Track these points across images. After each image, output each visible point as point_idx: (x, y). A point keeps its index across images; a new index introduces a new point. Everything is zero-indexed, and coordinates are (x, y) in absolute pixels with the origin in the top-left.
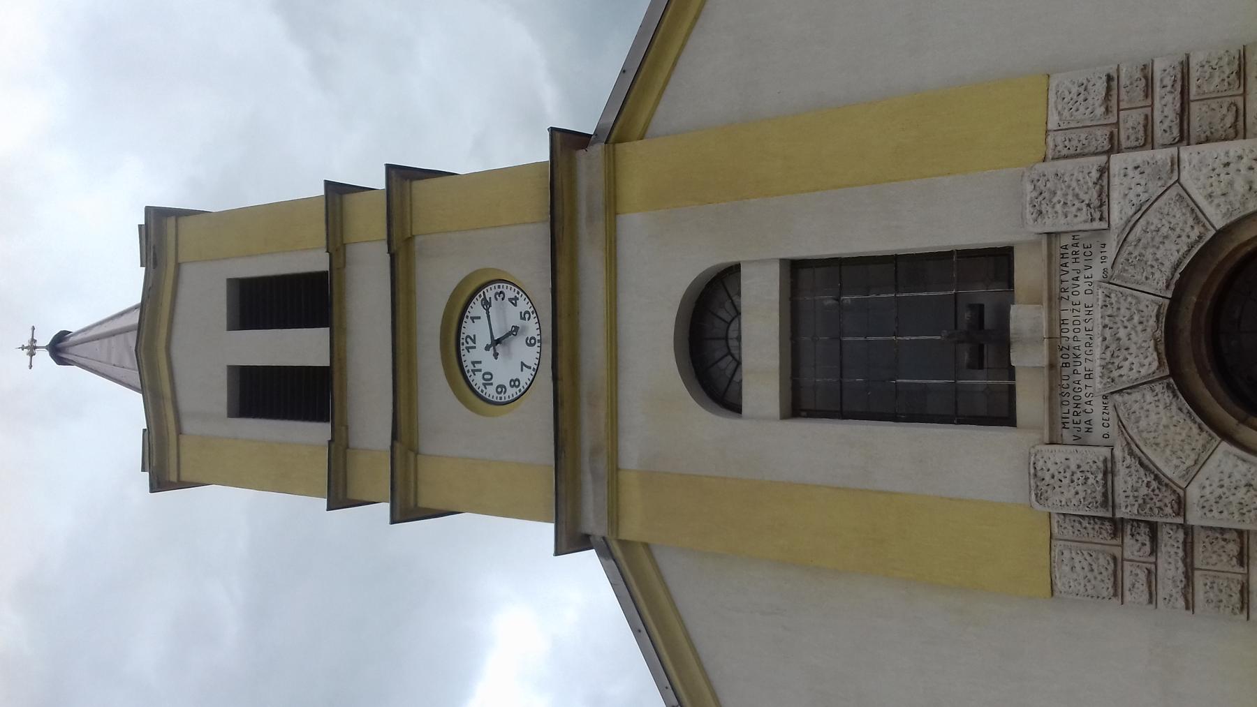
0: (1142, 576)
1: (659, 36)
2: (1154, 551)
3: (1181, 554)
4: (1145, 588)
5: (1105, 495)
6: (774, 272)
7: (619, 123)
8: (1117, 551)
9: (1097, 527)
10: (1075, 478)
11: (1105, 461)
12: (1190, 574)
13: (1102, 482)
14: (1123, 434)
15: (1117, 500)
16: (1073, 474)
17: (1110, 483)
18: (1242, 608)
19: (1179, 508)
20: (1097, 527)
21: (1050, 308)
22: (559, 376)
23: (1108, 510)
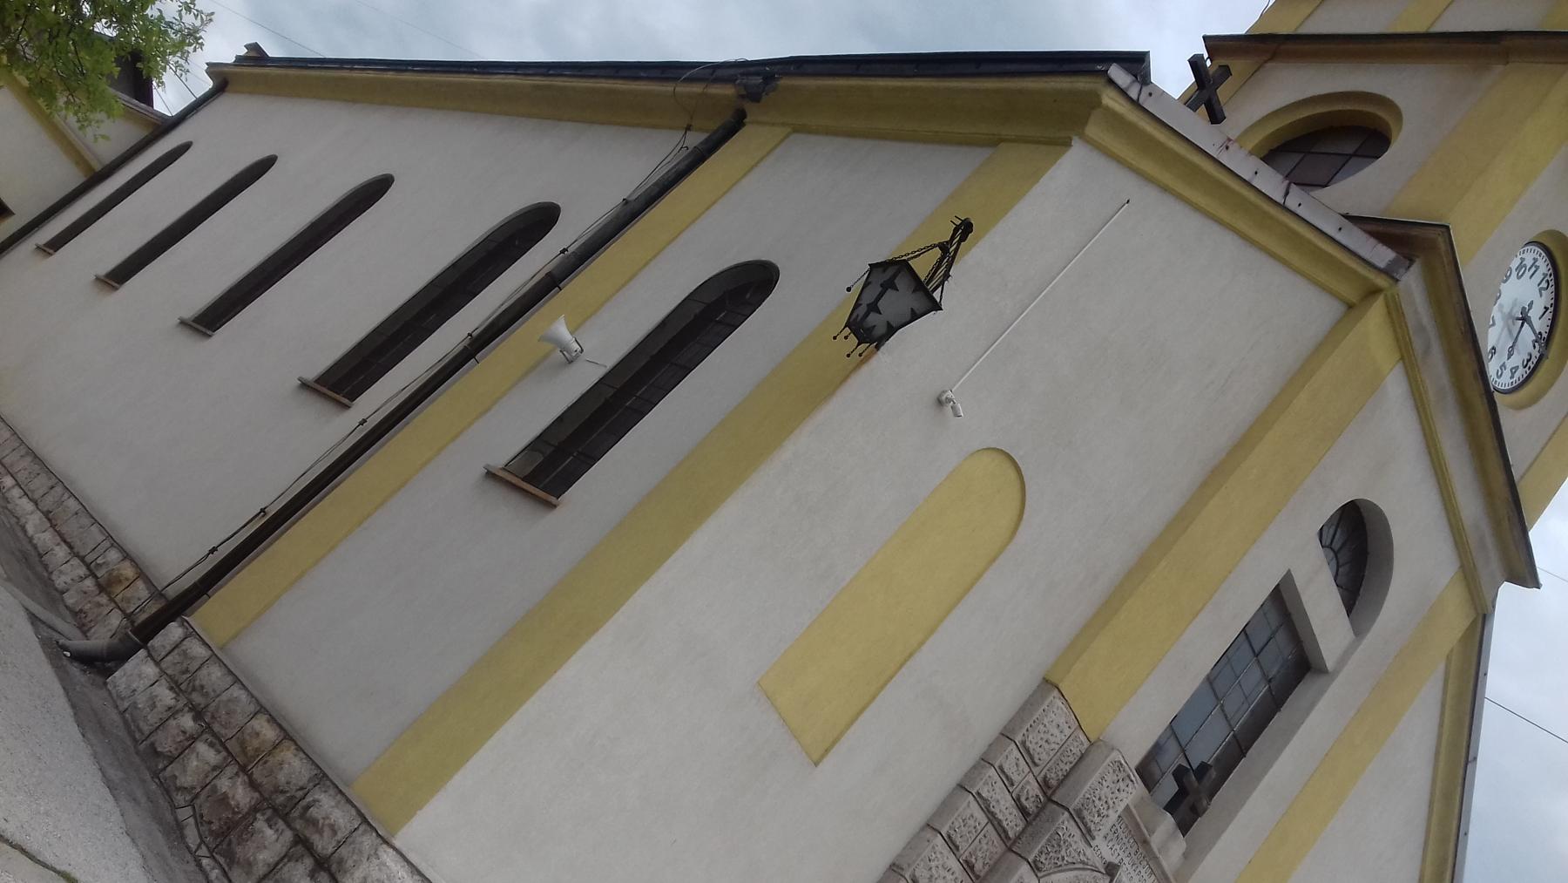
0: (1015, 778)
1: (1467, 724)
2: (1017, 801)
3: (1005, 824)
4: (1009, 774)
5: (1082, 819)
6: (1330, 658)
7: (1478, 635)
8: (1036, 770)
9: (1060, 773)
10: (1105, 806)
11: (1093, 838)
12: (989, 816)
13: (1089, 824)
14: (1091, 866)
15: (1072, 823)
16: (1108, 808)
17: (1082, 827)
18: (949, 837)
19: (1036, 865)
20: (1060, 773)
21: (1164, 873)
22: (1484, 397)
23: (1074, 810)
